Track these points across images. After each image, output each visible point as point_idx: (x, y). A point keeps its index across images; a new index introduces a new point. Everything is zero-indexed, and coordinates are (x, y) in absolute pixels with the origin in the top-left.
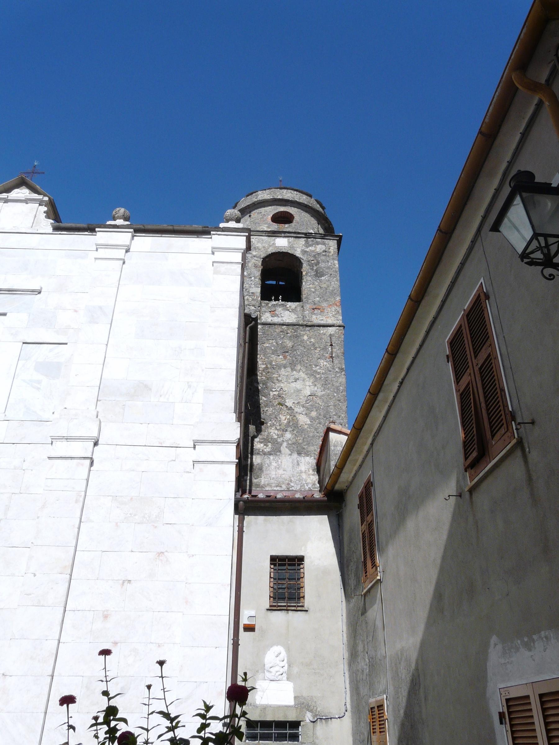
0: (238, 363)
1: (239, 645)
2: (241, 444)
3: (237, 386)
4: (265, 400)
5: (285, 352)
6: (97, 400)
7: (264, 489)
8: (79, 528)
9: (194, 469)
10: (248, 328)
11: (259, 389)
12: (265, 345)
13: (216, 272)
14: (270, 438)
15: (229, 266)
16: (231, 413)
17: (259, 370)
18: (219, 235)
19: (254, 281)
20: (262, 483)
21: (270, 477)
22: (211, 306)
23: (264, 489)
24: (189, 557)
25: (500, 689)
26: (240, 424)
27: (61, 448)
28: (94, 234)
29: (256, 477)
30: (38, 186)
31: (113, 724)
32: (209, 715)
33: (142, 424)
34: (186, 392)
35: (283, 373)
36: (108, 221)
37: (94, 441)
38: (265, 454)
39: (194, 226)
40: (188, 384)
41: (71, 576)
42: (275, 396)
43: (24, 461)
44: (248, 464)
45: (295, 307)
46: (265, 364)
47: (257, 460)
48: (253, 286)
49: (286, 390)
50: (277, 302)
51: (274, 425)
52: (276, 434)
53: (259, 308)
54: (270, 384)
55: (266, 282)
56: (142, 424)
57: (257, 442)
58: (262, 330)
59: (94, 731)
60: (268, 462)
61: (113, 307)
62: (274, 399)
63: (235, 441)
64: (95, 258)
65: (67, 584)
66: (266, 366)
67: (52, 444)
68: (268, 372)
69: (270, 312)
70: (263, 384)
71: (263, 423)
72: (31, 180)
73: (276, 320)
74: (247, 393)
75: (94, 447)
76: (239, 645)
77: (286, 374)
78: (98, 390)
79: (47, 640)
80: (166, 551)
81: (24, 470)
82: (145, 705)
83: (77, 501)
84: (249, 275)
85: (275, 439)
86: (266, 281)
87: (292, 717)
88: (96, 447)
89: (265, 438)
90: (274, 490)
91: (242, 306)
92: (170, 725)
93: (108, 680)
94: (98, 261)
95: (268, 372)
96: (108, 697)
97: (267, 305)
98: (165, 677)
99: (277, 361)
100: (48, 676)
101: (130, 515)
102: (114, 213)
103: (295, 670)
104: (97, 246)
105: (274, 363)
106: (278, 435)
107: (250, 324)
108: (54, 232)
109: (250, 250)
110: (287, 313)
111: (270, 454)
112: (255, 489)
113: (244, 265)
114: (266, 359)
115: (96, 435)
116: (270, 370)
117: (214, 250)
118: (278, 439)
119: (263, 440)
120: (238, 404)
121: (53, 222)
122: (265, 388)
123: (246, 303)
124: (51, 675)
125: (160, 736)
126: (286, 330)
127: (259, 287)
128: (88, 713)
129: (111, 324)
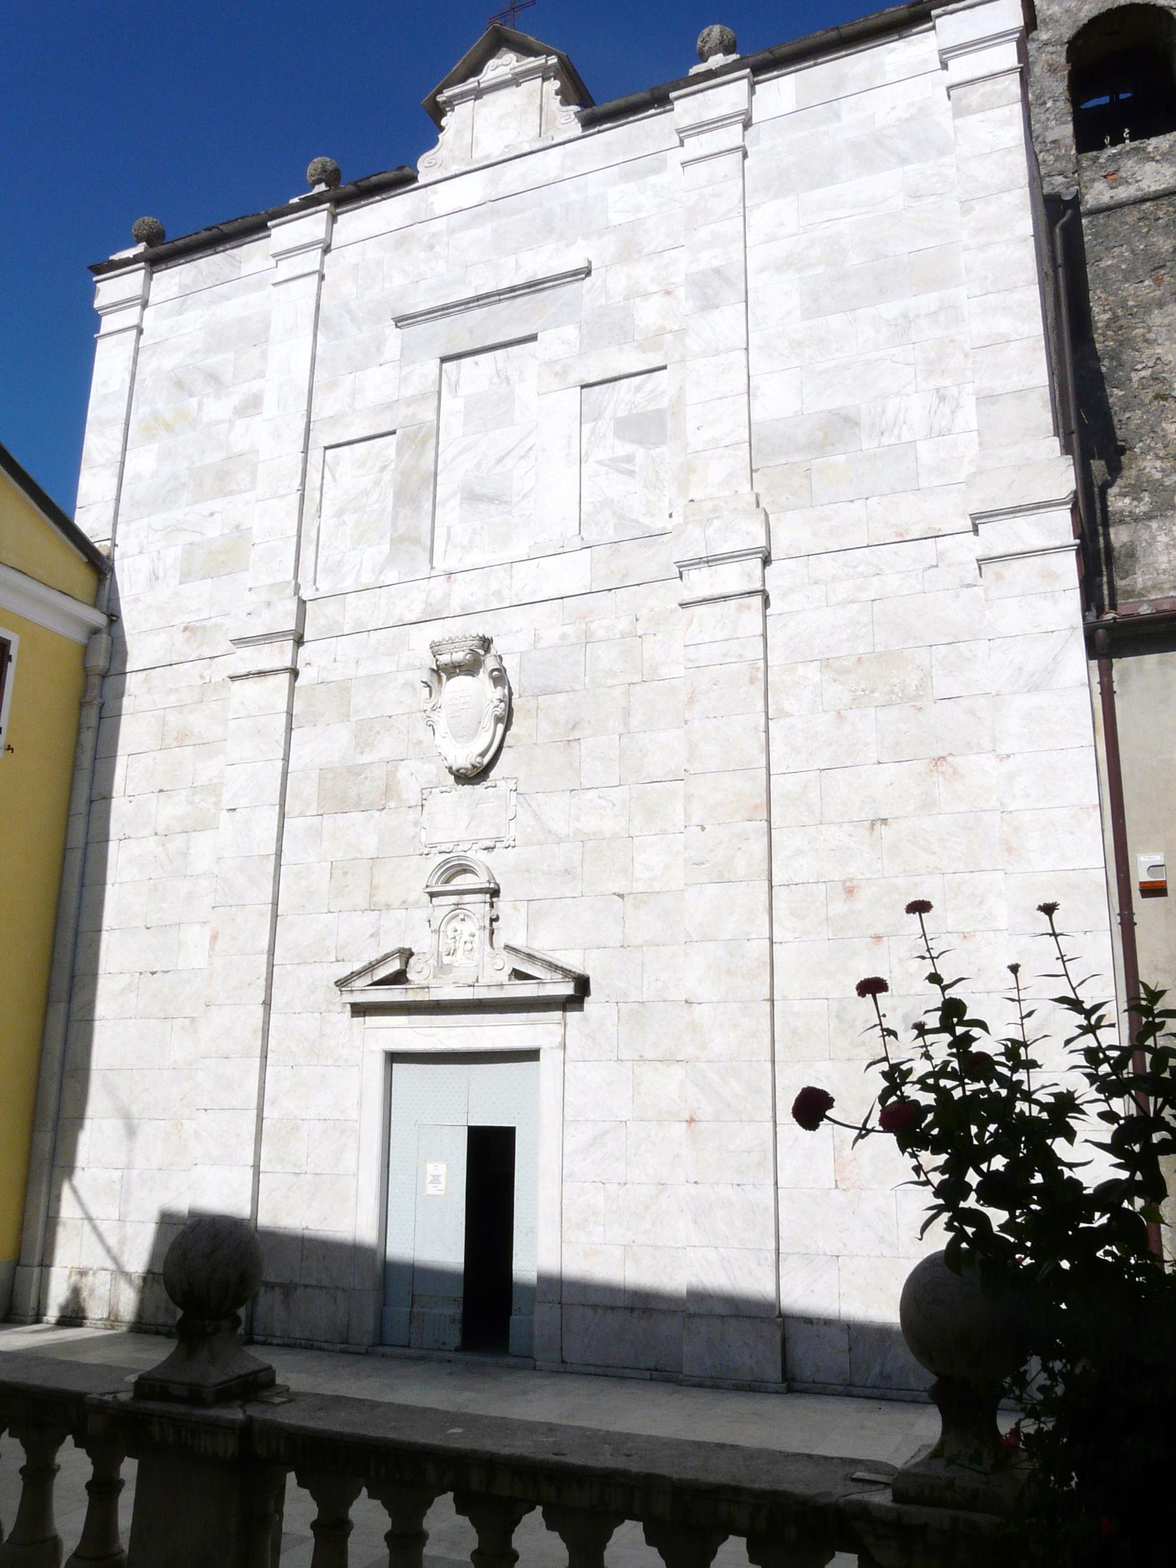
0: (1047, 320)
1: (1136, 924)
2: (1081, 504)
3: (1051, 374)
4: (1122, 396)
5: (1156, 268)
6: (752, 471)
7: (1144, 599)
8: (767, 732)
9: (981, 576)
10: (1057, 231)
11: (1101, 373)
12: (1103, 264)
13: (959, 112)
14: (1145, 480)
15: (987, 86)
16: (1048, 437)
17: (1098, 328)
18: (951, 13)
19: (1054, 111)
20: (1139, 586)
21: (1157, 570)
22: (963, 200)
23: (1144, 599)
24: (1001, 760)
26: (1074, 459)
27: (701, 582)
28: (668, 107)
29: (1122, 575)
30: (530, 38)
31: (960, 1030)
32: (1158, 1008)
33: (852, 501)
34: (936, 412)
35: (1158, 321)
36: (691, 68)
37: (760, 555)
38: (1137, 519)
39: (887, 10)
40: (938, 392)
41: (770, 822)
42: (1144, 381)
43: (637, 620)
44: (1099, 549)
45: (1171, 147)
46: (1110, 309)
47: (1119, 536)
48: (1053, 123)
49: (1172, 359)
50: (1119, 147)
51: (1150, 449)
52: (1159, 469)
53: (1076, 175)
54: (1128, 355)
55: (1082, 107)
56: (852, 501)
57: (1115, 496)
58: (1090, 229)
59: (920, 1049)
60: (1147, 537)
61: (743, 262)
62: (1142, 389)
63: (1067, 499)
64: (682, 164)
65: (766, 839)
66: (1114, 313)
67: (681, 577)
68: (1121, 328)
69: (1105, 177)
70: (1112, 359)
71: (1122, 451)
72: (514, 29)
73: (1123, 193)
74: (1077, 387)
75: (764, 568)
76: (1136, 924)
77: (1167, 321)
78: (748, 448)
79: (748, 940)
80: (950, 754)
81: (640, 637)
82: (1013, 1000)
83: (752, 681)
84: (1038, 98)
85: (1157, 480)
86: (1083, 103)
88: (767, 568)
89: (1133, 482)
90: (1168, 597)
91: (1036, 178)
92: (1085, 1023)
93: (933, 955)
94: (689, 169)
95: (1121, 328)
96: (940, 985)
97: (1094, 162)
98: (1062, 934)
99: (1137, 297)
100: (764, 1000)
101: (863, 693)
102: (699, 43)
104: (681, 135)
105: (1131, 303)
106: (1163, 470)
107: (1061, 218)
108: (588, 130)
109: (1035, 28)
110: (1150, 167)
111: (1151, 518)
112: (1123, 601)
113: (1025, 71)
114: (1110, 298)
115: (762, 542)
116: (1123, 322)
117: (944, 57)
118: (1166, 479)
119: (1127, 490)
120: (1059, 416)
121: (579, 109)
122: (1116, 367)
123: (1043, 172)
124: (770, 1000)
125: (1068, 1042)
126: (1152, 212)
127: (1066, 123)
128: (848, 1060)
129: (746, 302)
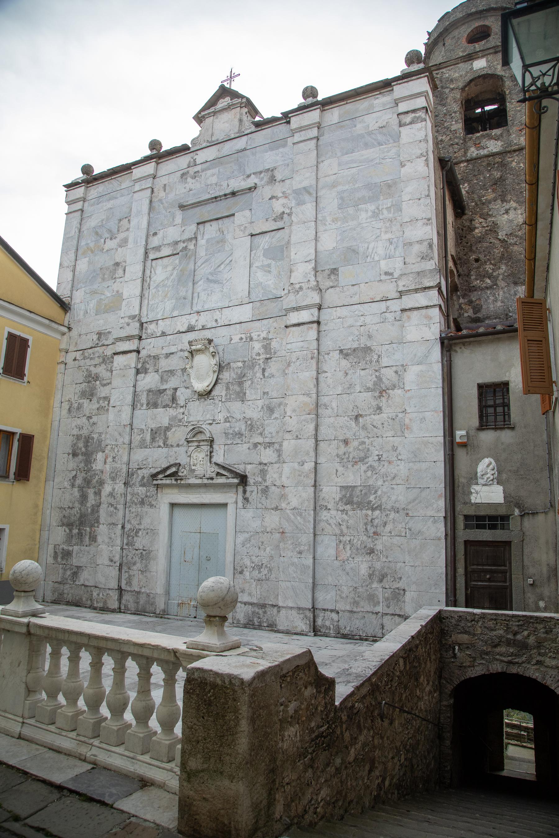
18: (400, 84)
25: (178, 512)
27: (294, 318)
73: (483, 152)
87: (502, 511)
103: (504, 476)
106: (493, 269)
